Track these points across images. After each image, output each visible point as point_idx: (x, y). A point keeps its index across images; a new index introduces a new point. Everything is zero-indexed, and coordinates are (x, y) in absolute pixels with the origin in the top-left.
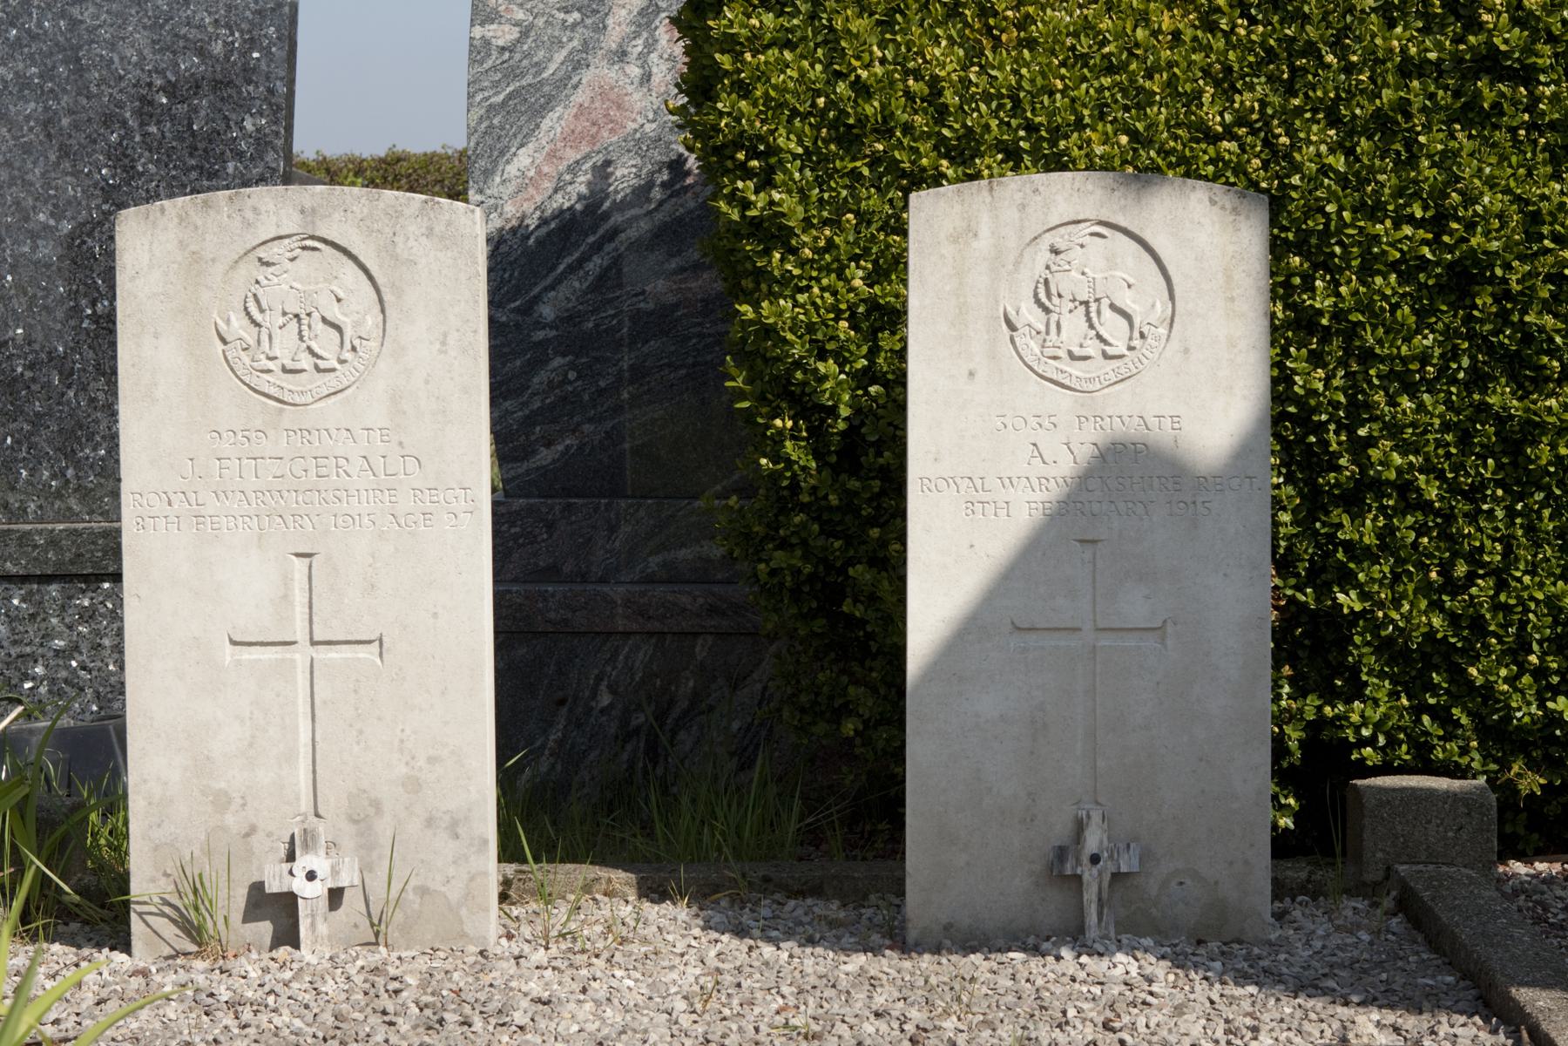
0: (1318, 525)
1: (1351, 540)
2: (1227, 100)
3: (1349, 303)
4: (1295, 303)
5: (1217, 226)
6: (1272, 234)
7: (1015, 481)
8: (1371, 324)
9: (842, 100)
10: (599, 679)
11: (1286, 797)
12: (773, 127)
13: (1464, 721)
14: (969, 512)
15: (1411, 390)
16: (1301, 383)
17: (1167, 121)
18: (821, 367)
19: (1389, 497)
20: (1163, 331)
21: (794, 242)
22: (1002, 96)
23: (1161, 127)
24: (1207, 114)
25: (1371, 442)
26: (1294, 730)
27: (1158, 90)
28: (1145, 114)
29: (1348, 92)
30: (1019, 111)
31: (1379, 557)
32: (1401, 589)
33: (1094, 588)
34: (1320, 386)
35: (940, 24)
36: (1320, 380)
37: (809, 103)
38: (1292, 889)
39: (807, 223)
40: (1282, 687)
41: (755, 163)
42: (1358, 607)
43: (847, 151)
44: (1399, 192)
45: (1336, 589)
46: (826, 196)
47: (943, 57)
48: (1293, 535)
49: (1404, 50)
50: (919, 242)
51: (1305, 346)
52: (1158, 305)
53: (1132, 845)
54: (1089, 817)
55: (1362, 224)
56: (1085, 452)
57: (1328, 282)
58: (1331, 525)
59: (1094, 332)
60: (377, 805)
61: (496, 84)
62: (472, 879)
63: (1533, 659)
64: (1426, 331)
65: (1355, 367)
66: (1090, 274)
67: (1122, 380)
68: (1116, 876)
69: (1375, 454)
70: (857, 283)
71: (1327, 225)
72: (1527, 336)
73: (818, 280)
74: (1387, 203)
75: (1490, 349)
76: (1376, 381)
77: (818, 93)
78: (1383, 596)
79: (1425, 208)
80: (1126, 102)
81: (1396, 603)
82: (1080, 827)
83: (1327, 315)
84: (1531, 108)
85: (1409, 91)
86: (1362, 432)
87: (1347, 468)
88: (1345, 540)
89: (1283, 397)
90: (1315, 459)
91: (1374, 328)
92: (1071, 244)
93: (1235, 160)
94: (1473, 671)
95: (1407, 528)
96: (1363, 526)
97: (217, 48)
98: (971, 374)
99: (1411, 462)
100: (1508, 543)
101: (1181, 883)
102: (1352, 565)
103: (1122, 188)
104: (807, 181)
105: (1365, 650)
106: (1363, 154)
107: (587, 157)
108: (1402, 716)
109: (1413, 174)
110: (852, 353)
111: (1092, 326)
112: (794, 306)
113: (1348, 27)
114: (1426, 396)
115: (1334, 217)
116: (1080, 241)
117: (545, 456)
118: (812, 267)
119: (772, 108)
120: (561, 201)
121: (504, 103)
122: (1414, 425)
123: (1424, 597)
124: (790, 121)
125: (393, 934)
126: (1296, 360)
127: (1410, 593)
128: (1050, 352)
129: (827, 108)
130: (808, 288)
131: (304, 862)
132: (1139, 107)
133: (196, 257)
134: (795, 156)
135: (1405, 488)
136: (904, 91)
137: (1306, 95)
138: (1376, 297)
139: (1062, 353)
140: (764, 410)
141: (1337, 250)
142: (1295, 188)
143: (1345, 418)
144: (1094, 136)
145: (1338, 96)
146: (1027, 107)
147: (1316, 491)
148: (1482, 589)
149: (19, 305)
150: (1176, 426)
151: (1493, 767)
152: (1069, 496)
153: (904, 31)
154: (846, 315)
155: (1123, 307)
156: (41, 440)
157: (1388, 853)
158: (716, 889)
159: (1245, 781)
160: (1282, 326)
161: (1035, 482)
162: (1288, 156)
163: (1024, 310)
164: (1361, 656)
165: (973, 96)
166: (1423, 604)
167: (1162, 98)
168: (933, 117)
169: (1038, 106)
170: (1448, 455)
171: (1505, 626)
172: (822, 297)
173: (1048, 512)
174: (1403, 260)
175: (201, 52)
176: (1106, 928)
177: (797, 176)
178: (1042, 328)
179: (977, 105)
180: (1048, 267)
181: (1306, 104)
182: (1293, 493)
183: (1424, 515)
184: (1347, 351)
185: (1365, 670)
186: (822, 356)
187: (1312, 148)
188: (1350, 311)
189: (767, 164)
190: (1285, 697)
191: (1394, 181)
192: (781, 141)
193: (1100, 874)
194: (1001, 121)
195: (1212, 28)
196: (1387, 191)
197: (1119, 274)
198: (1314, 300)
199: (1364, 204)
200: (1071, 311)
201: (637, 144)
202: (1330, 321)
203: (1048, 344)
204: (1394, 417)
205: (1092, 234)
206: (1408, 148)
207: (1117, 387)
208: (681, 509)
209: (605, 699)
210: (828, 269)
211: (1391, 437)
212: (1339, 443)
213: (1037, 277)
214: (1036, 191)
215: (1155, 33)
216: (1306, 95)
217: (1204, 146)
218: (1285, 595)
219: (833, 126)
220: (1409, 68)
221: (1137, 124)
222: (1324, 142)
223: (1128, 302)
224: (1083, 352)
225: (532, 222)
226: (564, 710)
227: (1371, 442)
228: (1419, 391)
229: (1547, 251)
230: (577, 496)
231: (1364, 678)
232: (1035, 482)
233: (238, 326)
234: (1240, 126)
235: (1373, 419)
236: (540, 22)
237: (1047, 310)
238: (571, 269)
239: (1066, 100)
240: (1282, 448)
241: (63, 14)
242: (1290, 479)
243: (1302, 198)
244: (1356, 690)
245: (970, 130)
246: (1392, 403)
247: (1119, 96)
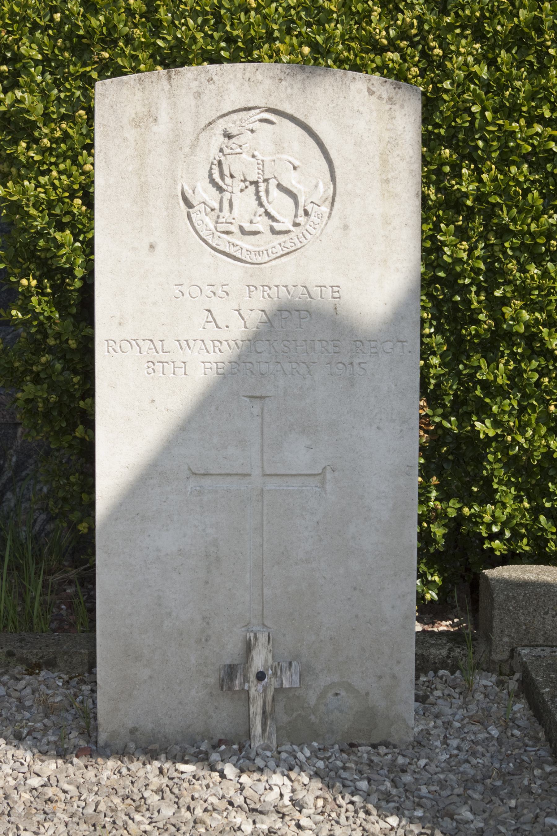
0: (461, 367)
1: (487, 380)
2: (392, 19)
4: (445, 188)
5: (375, 114)
6: (427, 130)
7: (191, 343)
8: (507, 206)
9: (73, 15)
11: (432, 575)
12: (18, 36)
14: (150, 370)
15: (538, 260)
16: (449, 253)
17: (342, 35)
18: (58, 236)
19: (519, 345)
20: (325, 209)
21: (36, 134)
22: (207, 13)
23: (337, 40)
24: (375, 29)
26: (439, 527)
27: (335, 9)
28: (324, 29)
29: (491, 12)
30: (220, 26)
31: (510, 393)
32: (526, 418)
33: (262, 438)
34: (464, 256)
36: (465, 250)
37: (48, 18)
38: (435, 663)
39: (46, 115)
40: (430, 492)
42: (491, 433)
43: (80, 58)
44: (532, 96)
45: (474, 418)
46: (62, 95)
48: (441, 375)
50: (104, 126)
51: (453, 223)
52: (321, 185)
53: (294, 664)
54: (256, 638)
55: (501, 122)
57: (473, 171)
58: (472, 367)
59: (263, 210)
64: (551, 212)
65: (493, 241)
66: (259, 156)
67: (288, 253)
68: (280, 690)
69: (508, 311)
71: (472, 123)
73: (56, 164)
74: (522, 105)
76: (510, 252)
78: (512, 424)
80: (308, 19)
81: (522, 429)
82: (249, 648)
83: (471, 198)
85: (541, 10)
86: (498, 293)
87: (485, 322)
88: (482, 380)
89: (435, 264)
90: (460, 314)
91: (509, 208)
92: (242, 130)
93: (397, 67)
95: (531, 371)
96: (497, 368)
98: (152, 247)
99: (537, 318)
101: (337, 694)
102: (487, 400)
103: (289, 79)
104: (47, 84)
105: (496, 466)
106: (502, 64)
108: (524, 516)
109: (543, 81)
110: (84, 226)
111: (261, 205)
112: (36, 187)
114: (550, 265)
115: (478, 116)
116: (251, 126)
118: (51, 154)
119: (17, 22)
122: (539, 288)
123: (544, 424)
124: (32, 31)
126: (445, 234)
127: (533, 422)
128: (223, 227)
129: (62, 23)
130: (49, 171)
132: (319, 23)
134: (37, 63)
136: (126, 9)
137: (457, 14)
138: (511, 183)
139: (234, 228)
140: (17, 271)
141: (480, 143)
142: (446, 91)
143: (485, 282)
144: (282, 48)
145: (483, 15)
146: (228, 23)
147: (461, 339)
150: (336, 295)
152: (239, 356)
154: (80, 194)
155: (289, 187)
157: (513, 638)
159: (393, 607)
160: (435, 206)
161: (209, 345)
162: (441, 66)
163: (199, 189)
164: (493, 470)
165: (182, 13)
166: (544, 430)
167: (338, 16)
168: (151, 31)
169: (236, 21)
172: (60, 179)
173: (221, 371)
174: (534, 152)
176: (269, 738)
177: (39, 79)
178: (216, 206)
179: (186, 20)
180: (221, 150)
181: (457, 22)
182: (441, 341)
183: (546, 360)
185: (496, 480)
186: (61, 227)
187: (460, 58)
188: (489, 194)
189: (15, 69)
190: (433, 500)
191: (528, 87)
192: (23, 50)
193: (265, 689)
194: (206, 34)
196: (522, 95)
197: (285, 157)
198: (461, 185)
199: (502, 105)
200: (242, 191)
202: (474, 202)
203: (221, 220)
204: (523, 282)
205: (261, 121)
206: (539, 59)
207: (283, 259)
208: (9, 334)
210: (64, 156)
211: (522, 297)
212: (479, 302)
213: (211, 159)
214: (210, 80)
216: (456, 13)
217: (372, 56)
218: (434, 422)
219: (68, 37)
221: (317, 37)
222: (470, 54)
223: (294, 183)
224: (253, 228)
227: (504, 301)
228: (544, 260)
231: (495, 486)
232: (209, 345)
234: (402, 40)
235: (508, 283)
237: (220, 189)
239: (259, 16)
240: (433, 305)
242: (439, 330)
243: (452, 100)
246: (523, 270)
247: (303, 14)
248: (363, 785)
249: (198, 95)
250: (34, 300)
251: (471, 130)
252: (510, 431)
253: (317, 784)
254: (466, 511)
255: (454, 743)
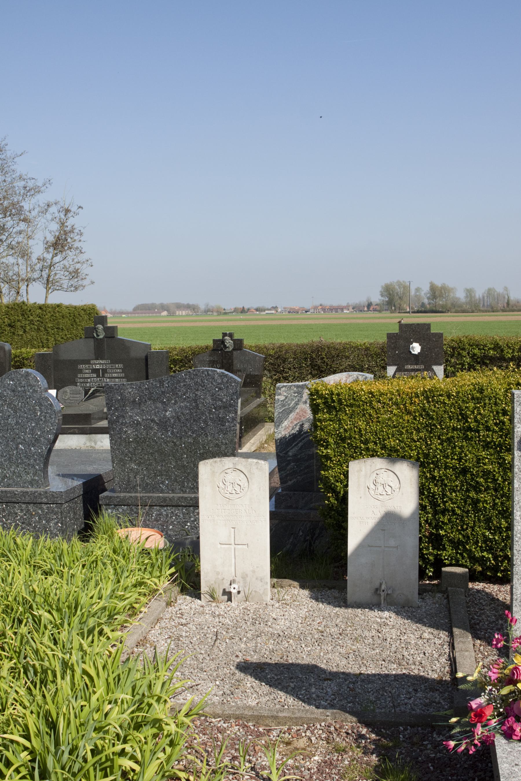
3: (442, 475)
10: (300, 530)
13: (466, 556)
15: (455, 492)
20: (398, 490)
25: (446, 502)
35: (361, 417)
39: (335, 456)
41: (325, 444)
42: (444, 534)
47: (362, 424)
49: (453, 425)
56: (383, 513)
60: (247, 575)
61: (280, 408)
62: (265, 589)
63: (480, 544)
68: (387, 594)
69: (447, 504)
70: (345, 468)
72: (477, 482)
75: (471, 485)
77: (337, 431)
79: (457, 456)
81: (452, 533)
84: (479, 437)
86: (445, 500)
94: (467, 547)
97: (224, 400)
100: (474, 522)
107: (299, 423)
113: (442, 421)
117: (290, 483)
120: (293, 432)
121: (282, 412)
124: (331, 436)
125: (250, 599)
131: (233, 586)
133: (214, 472)
135: (453, 511)
148: (469, 531)
149: (185, 451)
151: (472, 565)
153: (354, 419)
156: (189, 477)
158: (315, 587)
166: (457, 533)
170: (462, 505)
171: (474, 538)
175: (222, 401)
177: (333, 446)
184: (442, 484)
186: (338, 482)
195: (415, 419)
201: (308, 420)
209: (301, 533)
210: (339, 465)
215: (404, 420)
220: (454, 429)
225: (287, 436)
226: (293, 536)
227: (446, 502)
229: (481, 466)
230: (296, 491)
233: (221, 485)
236: (289, 395)
238: (295, 445)
241: (194, 393)
244: (444, 549)
245: (367, 439)
246: (451, 494)
248: (405, 614)
249: (371, 466)
250: (331, 499)
251: (437, 461)
252: (449, 533)
253: (394, 614)
254: (439, 552)
255: (427, 607)
